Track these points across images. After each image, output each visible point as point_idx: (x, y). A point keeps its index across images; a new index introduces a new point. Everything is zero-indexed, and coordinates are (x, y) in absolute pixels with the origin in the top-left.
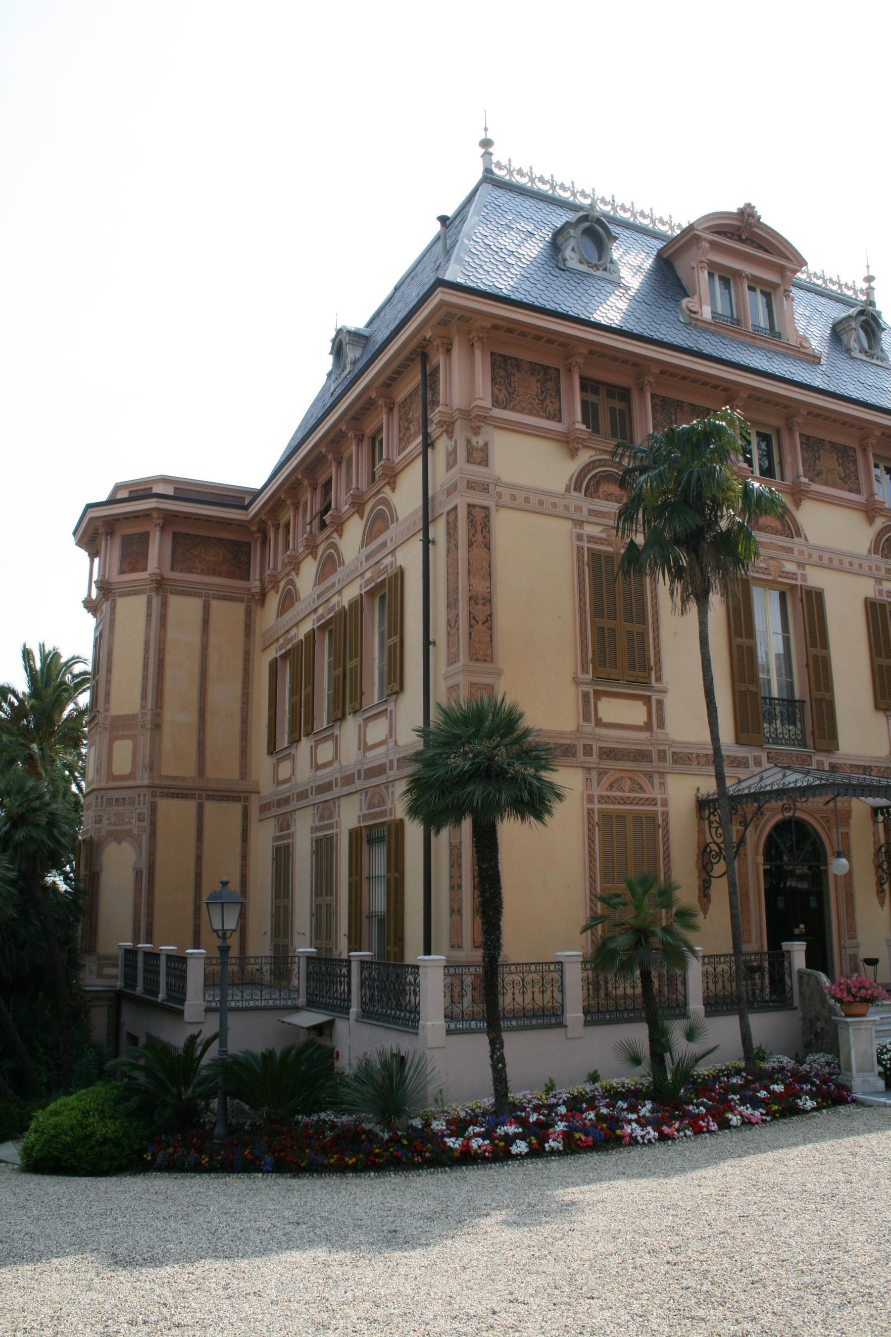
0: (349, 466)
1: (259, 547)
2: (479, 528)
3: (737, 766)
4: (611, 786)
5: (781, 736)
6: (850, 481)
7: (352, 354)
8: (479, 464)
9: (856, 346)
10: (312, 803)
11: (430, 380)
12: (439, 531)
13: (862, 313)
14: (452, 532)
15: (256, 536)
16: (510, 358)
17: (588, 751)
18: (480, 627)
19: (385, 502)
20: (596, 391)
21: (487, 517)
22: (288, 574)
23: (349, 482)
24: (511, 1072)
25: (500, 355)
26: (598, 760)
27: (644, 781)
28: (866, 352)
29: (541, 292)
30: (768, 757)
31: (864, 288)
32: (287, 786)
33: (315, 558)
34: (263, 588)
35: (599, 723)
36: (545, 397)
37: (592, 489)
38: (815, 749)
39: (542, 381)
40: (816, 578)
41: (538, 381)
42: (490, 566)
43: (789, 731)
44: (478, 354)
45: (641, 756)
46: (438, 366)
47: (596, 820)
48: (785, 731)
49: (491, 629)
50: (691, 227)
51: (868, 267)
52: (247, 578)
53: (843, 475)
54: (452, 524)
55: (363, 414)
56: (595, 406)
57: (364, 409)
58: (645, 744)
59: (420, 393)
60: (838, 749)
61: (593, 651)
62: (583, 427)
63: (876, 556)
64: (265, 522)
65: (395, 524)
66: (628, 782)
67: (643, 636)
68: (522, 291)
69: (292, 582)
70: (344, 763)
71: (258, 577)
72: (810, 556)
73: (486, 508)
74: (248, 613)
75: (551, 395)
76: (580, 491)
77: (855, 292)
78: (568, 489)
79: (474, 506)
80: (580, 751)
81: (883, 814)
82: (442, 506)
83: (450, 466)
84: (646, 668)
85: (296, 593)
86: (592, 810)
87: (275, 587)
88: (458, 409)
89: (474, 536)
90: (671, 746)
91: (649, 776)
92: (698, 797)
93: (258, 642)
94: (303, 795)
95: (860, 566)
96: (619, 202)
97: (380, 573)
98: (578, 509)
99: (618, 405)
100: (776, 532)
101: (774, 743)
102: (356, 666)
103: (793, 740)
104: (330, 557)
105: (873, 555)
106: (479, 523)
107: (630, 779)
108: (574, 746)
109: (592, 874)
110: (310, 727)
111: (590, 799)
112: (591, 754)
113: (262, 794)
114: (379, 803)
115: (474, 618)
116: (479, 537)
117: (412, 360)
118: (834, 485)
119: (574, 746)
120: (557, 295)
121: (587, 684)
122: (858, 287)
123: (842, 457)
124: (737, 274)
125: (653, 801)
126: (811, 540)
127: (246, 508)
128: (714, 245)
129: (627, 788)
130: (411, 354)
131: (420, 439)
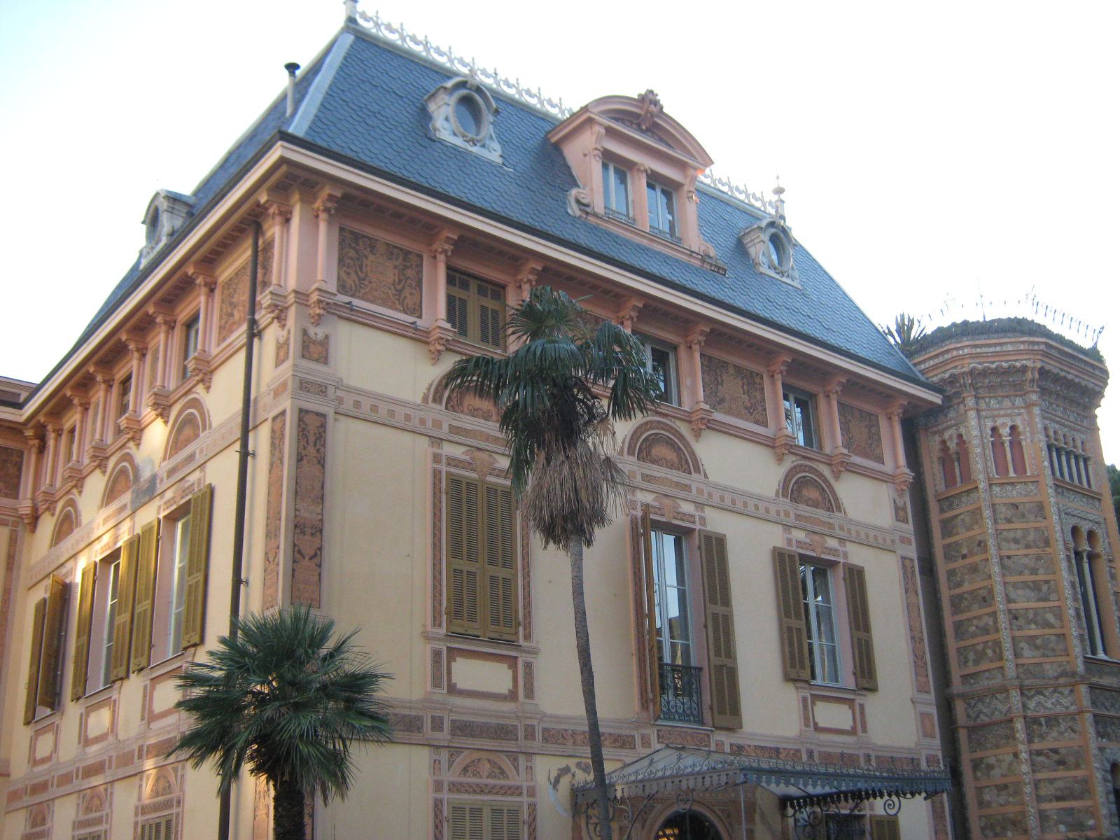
0: (155, 359)
1: (33, 457)
2: (312, 439)
3: (622, 747)
4: (465, 770)
5: (674, 710)
6: (756, 412)
7: (166, 224)
8: (317, 360)
9: (765, 260)
10: (77, 789)
11: (261, 258)
12: (261, 440)
13: (772, 224)
14: (277, 442)
15: (32, 442)
16: (364, 236)
17: (437, 724)
18: (306, 562)
19: (196, 403)
20: (464, 286)
21: (323, 426)
22: (68, 492)
23: (153, 378)
24: (624, 194)
25: (351, 232)
26: (449, 737)
27: (506, 763)
28: (775, 269)
29: (405, 162)
30: (658, 735)
31: (773, 201)
32: (46, 766)
33: (104, 473)
34: (35, 509)
35: (452, 689)
36: (404, 287)
37: (454, 403)
38: (714, 727)
39: (401, 267)
40: (717, 522)
41: (395, 267)
42: (323, 487)
43: (683, 704)
44: (323, 227)
45: (503, 732)
46: (273, 240)
47: (445, 813)
48: (679, 704)
49: (320, 566)
50: (585, 109)
51: (778, 178)
52: (16, 496)
53: (749, 405)
54: (278, 434)
55: (177, 296)
56: (463, 303)
57: (174, 291)
58: (509, 718)
59: (249, 272)
60: (741, 727)
61: (448, 600)
62: (448, 326)
63: (785, 500)
64: (43, 427)
65: (207, 432)
66: (487, 766)
67: (509, 583)
68: (382, 158)
69: (72, 503)
70: (122, 736)
71: (29, 495)
72: (710, 495)
73: (323, 416)
74: (13, 541)
75: (410, 286)
76: (440, 403)
77: (764, 204)
78: (425, 399)
79: (307, 412)
80: (428, 724)
81: (793, 806)
82: (267, 409)
83: (279, 362)
84: (510, 620)
85: (77, 518)
86: (441, 801)
87: (51, 509)
88: (295, 291)
89: (305, 448)
90: (541, 720)
91: (513, 756)
92: (573, 785)
93: (24, 578)
94: (66, 779)
95: (767, 510)
96: (501, 76)
97: (185, 491)
98: (437, 424)
99: (490, 304)
100: (672, 466)
101: (665, 719)
102: (145, 611)
103: (688, 716)
104: (123, 472)
105: (781, 499)
106: (311, 432)
107: (489, 760)
108: (420, 718)
109: (437, 832)
110: (80, 689)
111: (438, 786)
112: (441, 729)
113: (13, 777)
114: (164, 789)
115: (299, 552)
116: (311, 450)
117: (242, 231)
118: (738, 416)
119: (420, 718)
120: (425, 168)
121: (439, 640)
122: (767, 199)
123: (748, 385)
124: (631, 165)
125: (517, 791)
126: (712, 477)
127: (20, 406)
128: (610, 132)
129: (485, 774)
130: (241, 222)
131: (244, 327)
